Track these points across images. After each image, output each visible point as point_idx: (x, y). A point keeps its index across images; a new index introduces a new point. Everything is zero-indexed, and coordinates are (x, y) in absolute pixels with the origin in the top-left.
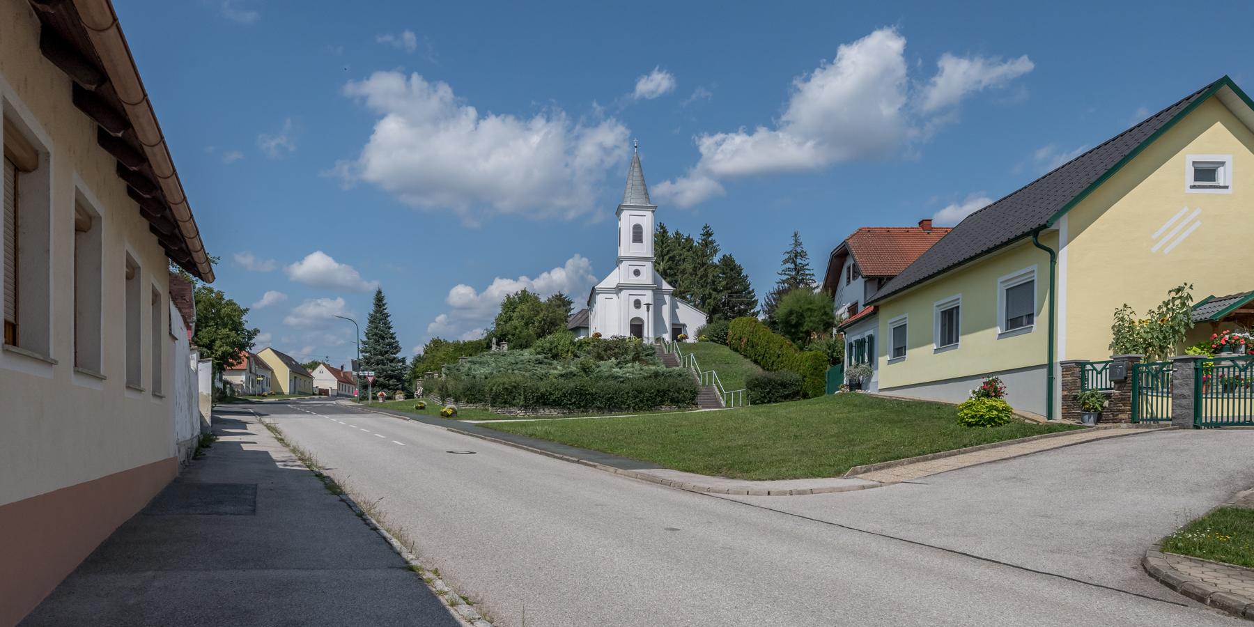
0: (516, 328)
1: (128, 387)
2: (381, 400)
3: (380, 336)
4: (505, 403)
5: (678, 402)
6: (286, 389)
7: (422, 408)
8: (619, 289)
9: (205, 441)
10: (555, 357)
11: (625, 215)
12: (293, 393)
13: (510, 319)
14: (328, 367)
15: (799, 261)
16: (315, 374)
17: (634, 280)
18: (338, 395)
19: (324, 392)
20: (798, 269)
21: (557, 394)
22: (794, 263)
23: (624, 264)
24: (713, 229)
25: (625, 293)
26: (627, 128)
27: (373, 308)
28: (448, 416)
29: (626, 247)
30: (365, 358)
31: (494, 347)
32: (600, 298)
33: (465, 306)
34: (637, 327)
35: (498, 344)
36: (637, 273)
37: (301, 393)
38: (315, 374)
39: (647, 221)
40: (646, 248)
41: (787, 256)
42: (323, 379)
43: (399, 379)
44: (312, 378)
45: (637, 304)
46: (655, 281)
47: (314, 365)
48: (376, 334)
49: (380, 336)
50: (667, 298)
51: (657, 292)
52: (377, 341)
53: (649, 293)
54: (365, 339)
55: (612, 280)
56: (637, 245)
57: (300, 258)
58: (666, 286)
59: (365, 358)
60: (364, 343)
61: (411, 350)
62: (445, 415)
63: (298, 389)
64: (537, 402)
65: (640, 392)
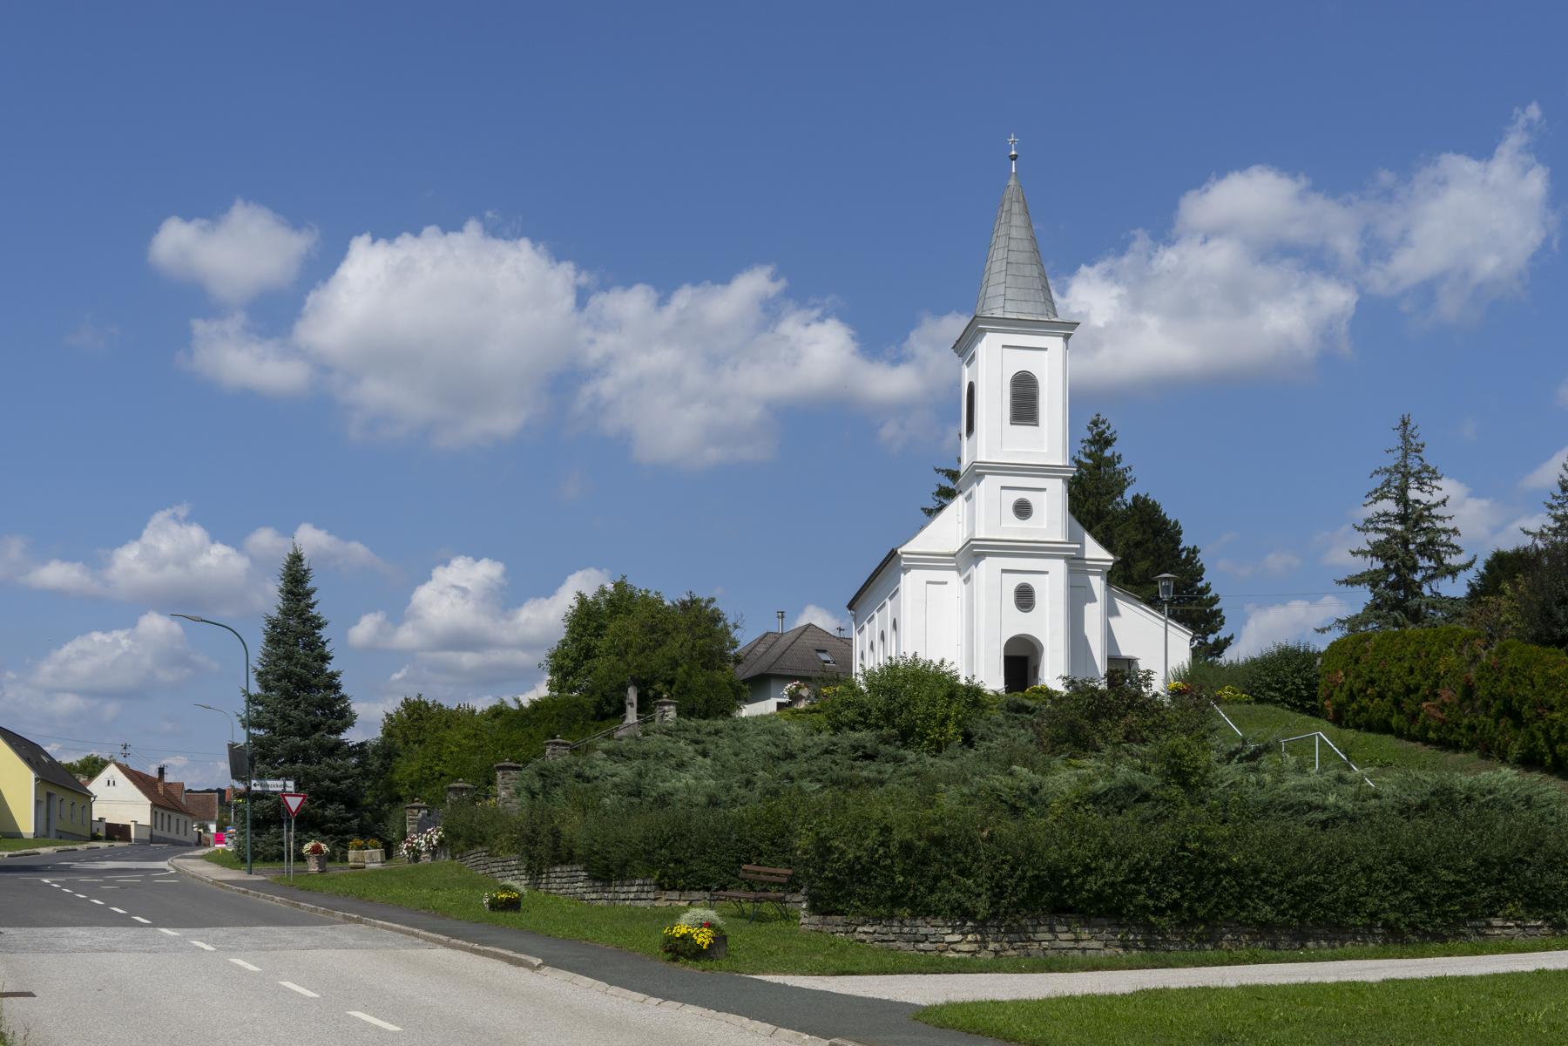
0: (675, 664)
2: (313, 866)
3: (297, 676)
4: (895, 901)
5: (1549, 905)
6: (25, 819)
7: (513, 905)
8: (973, 553)
10: (907, 736)
11: (989, 347)
12: (45, 832)
13: (588, 653)
14: (119, 766)
15: (1413, 494)
16: (96, 786)
18: (153, 839)
19: (117, 832)
20: (1412, 517)
21: (1112, 872)
22: (1402, 499)
23: (987, 489)
24: (1116, 425)
25: (988, 569)
27: (279, 602)
28: (698, 954)
29: (992, 436)
30: (257, 742)
31: (632, 716)
32: (911, 583)
33: (460, 629)
34: (1021, 661)
35: (644, 707)
36: (1023, 510)
37: (62, 836)
38: (96, 786)
40: (1049, 441)
41: (1379, 481)
42: (118, 801)
43: (351, 803)
44: (88, 797)
45: (1025, 598)
46: (1073, 538)
47: (93, 767)
48: (287, 675)
49: (297, 676)
50: (1097, 583)
51: (1077, 565)
52: (287, 694)
53: (1058, 568)
54: (255, 689)
55: (947, 531)
56: (1024, 430)
57: (207, 208)
58: (1095, 551)
59: (257, 742)
60: (252, 700)
61: (368, 720)
62: (682, 950)
63: (57, 824)
64: (1029, 903)
65: (1416, 868)
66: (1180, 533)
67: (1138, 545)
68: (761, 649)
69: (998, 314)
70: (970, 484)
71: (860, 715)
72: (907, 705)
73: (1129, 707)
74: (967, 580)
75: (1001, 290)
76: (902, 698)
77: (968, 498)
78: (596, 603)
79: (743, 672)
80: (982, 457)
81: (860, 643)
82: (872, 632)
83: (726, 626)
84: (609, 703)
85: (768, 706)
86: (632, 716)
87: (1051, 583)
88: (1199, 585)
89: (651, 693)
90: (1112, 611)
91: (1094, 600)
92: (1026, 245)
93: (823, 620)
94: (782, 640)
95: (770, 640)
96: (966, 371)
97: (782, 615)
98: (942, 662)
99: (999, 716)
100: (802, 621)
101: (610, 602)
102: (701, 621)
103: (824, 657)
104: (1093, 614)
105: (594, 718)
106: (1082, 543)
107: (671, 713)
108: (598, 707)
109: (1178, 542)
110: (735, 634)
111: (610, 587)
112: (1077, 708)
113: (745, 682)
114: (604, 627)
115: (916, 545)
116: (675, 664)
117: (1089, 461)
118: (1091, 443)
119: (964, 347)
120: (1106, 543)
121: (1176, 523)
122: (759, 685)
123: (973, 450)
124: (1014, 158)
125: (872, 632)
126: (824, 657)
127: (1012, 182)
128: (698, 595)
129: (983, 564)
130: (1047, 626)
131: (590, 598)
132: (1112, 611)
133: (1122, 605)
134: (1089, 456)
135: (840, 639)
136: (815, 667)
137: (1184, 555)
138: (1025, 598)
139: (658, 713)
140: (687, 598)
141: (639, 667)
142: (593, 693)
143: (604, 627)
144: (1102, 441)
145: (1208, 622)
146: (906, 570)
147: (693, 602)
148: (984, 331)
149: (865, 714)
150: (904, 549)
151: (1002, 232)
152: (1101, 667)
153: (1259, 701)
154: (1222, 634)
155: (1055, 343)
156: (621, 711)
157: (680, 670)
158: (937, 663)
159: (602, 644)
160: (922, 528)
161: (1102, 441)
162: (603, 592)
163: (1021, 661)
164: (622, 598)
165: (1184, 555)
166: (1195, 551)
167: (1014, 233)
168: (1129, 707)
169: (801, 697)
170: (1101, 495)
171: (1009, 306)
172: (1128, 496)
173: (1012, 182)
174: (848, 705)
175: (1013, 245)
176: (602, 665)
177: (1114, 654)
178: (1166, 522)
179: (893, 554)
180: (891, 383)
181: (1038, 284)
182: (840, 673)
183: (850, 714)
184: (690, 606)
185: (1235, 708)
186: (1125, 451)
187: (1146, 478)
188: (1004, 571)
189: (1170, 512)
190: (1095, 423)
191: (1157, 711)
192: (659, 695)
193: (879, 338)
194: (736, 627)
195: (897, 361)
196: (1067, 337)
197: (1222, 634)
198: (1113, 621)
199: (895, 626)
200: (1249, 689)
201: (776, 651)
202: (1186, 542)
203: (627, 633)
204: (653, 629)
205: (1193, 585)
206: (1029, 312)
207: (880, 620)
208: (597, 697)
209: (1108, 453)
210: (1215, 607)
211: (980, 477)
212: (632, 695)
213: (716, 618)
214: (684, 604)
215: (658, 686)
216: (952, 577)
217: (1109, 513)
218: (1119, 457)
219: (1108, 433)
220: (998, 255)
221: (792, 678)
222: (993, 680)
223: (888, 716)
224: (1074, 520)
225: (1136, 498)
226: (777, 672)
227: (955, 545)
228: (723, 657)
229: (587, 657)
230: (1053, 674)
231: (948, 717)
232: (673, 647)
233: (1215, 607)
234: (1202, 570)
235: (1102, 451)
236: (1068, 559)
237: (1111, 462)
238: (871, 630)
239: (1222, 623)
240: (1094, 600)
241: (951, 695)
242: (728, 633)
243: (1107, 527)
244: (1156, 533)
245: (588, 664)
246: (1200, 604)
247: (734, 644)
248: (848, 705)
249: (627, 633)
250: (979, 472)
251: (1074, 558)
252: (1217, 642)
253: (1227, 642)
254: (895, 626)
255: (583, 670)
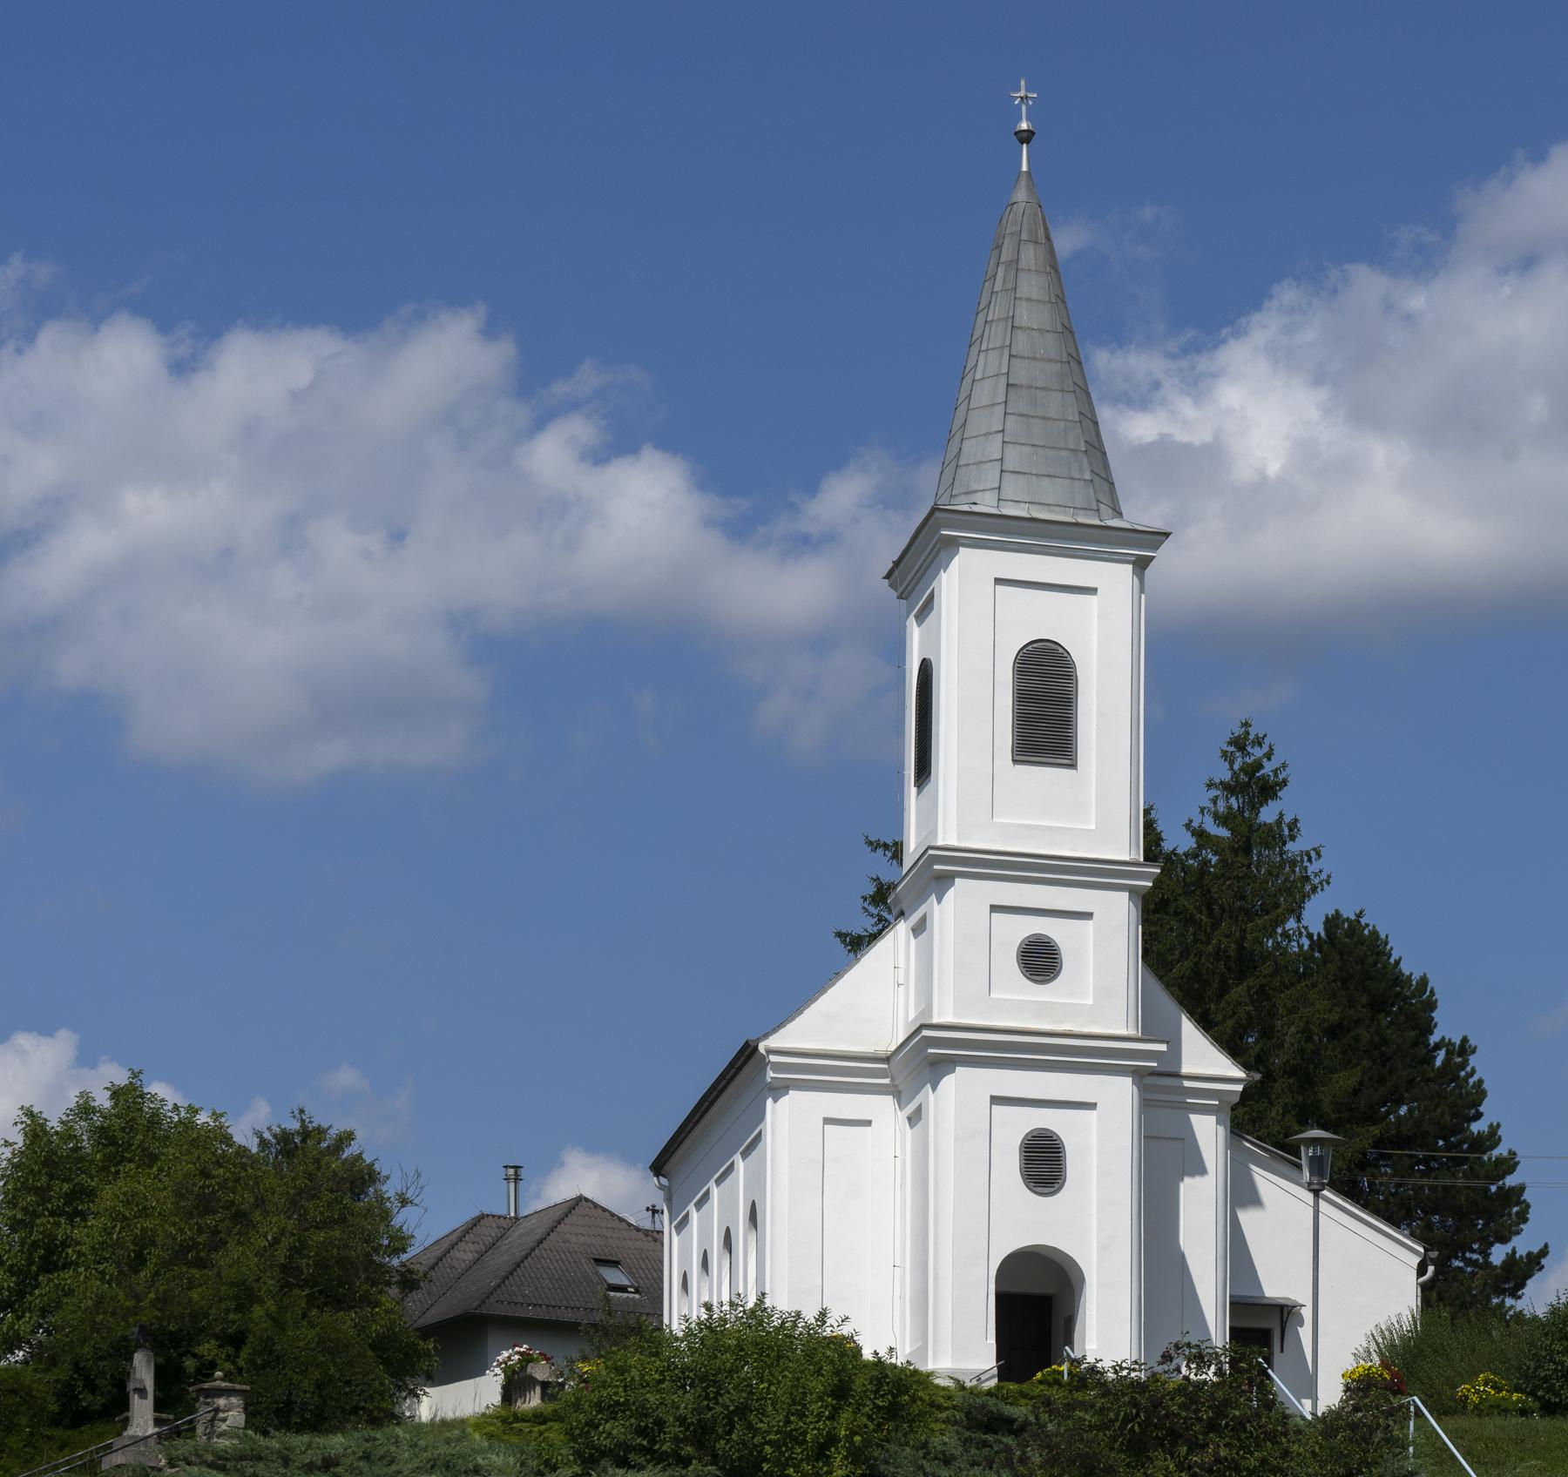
0: (246, 1296)
1: (1015, 761)
8: (926, 1058)
9: (1038, 272)
11: (965, 578)
13: (50, 1257)
17: (1020, 1005)
23: (958, 911)
24: (1288, 753)
25: (962, 1091)
26: (489, 332)
29: (974, 792)
31: (142, 1418)
32: (789, 1120)
34: (1034, 1303)
35: (171, 1399)
36: (1040, 960)
39: (1100, 622)
40: (1095, 805)
45: (1043, 1163)
46: (1152, 1026)
50: (1208, 1132)
51: (1161, 1090)
53: (1117, 1096)
55: (868, 1004)
58: (1204, 1059)
66: (1431, 1005)
67: (1334, 1032)
68: (465, 1254)
69: (987, 504)
70: (922, 898)
71: (641, 1432)
72: (742, 1410)
73: (1212, 1426)
74: (915, 1119)
75: (994, 448)
76: (731, 1398)
77: (919, 929)
78: (68, 1134)
79: (421, 1309)
80: (948, 836)
81: (678, 1252)
82: (729, 1206)
83: (381, 1200)
84: (92, 1387)
85: (471, 1397)
86: (142, 1418)
87: (1102, 1130)
88: (1477, 1127)
89: (190, 1364)
90: (1241, 1194)
91: (1202, 1171)
92: (1050, 345)
93: (610, 1182)
94: (514, 1235)
95: (488, 1232)
96: (915, 633)
97: (515, 1175)
98: (823, 1316)
99: (946, 1439)
100: (560, 1190)
101: (104, 1135)
102: (321, 1182)
103: (614, 1276)
104: (1199, 1203)
105: (55, 1421)
106: (1174, 1042)
107: (233, 1415)
108: (66, 1395)
109: (1429, 1028)
110: (404, 1219)
111: (103, 1100)
112: (1103, 1427)
113: (426, 1332)
114: (90, 1194)
115: (801, 1034)
116: (246, 1296)
117: (1224, 833)
118: (1229, 789)
119: (912, 575)
120: (1232, 1046)
121: (1424, 982)
122: (456, 1344)
123: (929, 818)
124: (1026, 137)
125: (729, 1206)
126: (614, 1276)
127: (1021, 195)
128: (319, 1119)
129: (949, 1082)
130: (1093, 1226)
131: (54, 1124)
132: (1241, 1194)
133: (1267, 1182)
134: (1223, 820)
135: (646, 1233)
136: (579, 1294)
137: (1441, 1056)
138: (1043, 1163)
139: (203, 1412)
140: (294, 1126)
141: (163, 1301)
142: (54, 1362)
143: (90, 1194)
144: (1254, 786)
145: (1490, 1216)
146: (779, 1090)
147: (306, 1134)
148: (953, 545)
149: (650, 1430)
150: (774, 1042)
151: (996, 312)
152: (1216, 1327)
153: (1549, 1409)
154: (1523, 1244)
155: (1114, 579)
156: (118, 1408)
157: (258, 1311)
158: (810, 1315)
159: (87, 1234)
160: (838, 975)
161: (1254, 786)
162: (85, 1109)
163: (1034, 1303)
164: (131, 1127)
165: (1441, 1056)
166: (1465, 1049)
167: (1024, 316)
168: (1212, 1426)
169: (531, 1382)
170: (1250, 915)
171: (1012, 486)
172: (1314, 917)
173: (1021, 195)
174: (613, 1410)
175: (1022, 343)
176: (83, 1285)
177: (1246, 1292)
178: (1399, 980)
179: (748, 1054)
180: (782, 592)
181: (1076, 439)
182: (638, 1321)
183: (617, 1430)
184: (302, 1149)
185: (1492, 1425)
186: (1308, 810)
187: (1358, 870)
188: (996, 1100)
189: (1411, 956)
190: (1239, 744)
191: (1272, 1437)
192: (206, 1369)
193: (753, 486)
194: (404, 1202)
195: (804, 545)
196: (1141, 565)
197: (1523, 1244)
198: (1246, 1218)
199: (753, 1217)
200: (1528, 1382)
201: (500, 1260)
202: (1447, 1026)
203: (144, 1212)
204: (205, 1204)
205: (1459, 1129)
206: (1054, 501)
207: (722, 1203)
208: (62, 1373)
209: (1268, 814)
210: (1510, 1181)
211: (943, 882)
212: (143, 1369)
213: (362, 1178)
214: (284, 1138)
215: (207, 1349)
216: (882, 1108)
217: (1266, 956)
218: (1293, 825)
219: (1268, 768)
220: (988, 364)
221: (517, 1326)
222: (963, 1350)
223: (701, 1435)
224: (1157, 989)
225: (1333, 922)
226: (500, 1310)
227: (888, 1035)
228: (379, 1275)
229: (48, 1266)
230: (1107, 1335)
231: (832, 1440)
232: (240, 1258)
233: (1510, 1181)
234: (1480, 1093)
235: (1255, 808)
236: (1138, 1075)
237: (1275, 836)
238: (704, 1225)
239: (1523, 1218)
240: (1202, 1171)
241: (841, 1392)
242: (386, 1216)
243: (1262, 990)
244: (1378, 1005)
245: (46, 1287)
246: (1472, 1174)
247: (400, 1242)
248: (613, 1410)
249: (144, 1212)
250: (942, 870)
251: (1153, 1073)
252: (1511, 1260)
253: (1534, 1262)
254: (753, 1217)
255: (38, 1297)
